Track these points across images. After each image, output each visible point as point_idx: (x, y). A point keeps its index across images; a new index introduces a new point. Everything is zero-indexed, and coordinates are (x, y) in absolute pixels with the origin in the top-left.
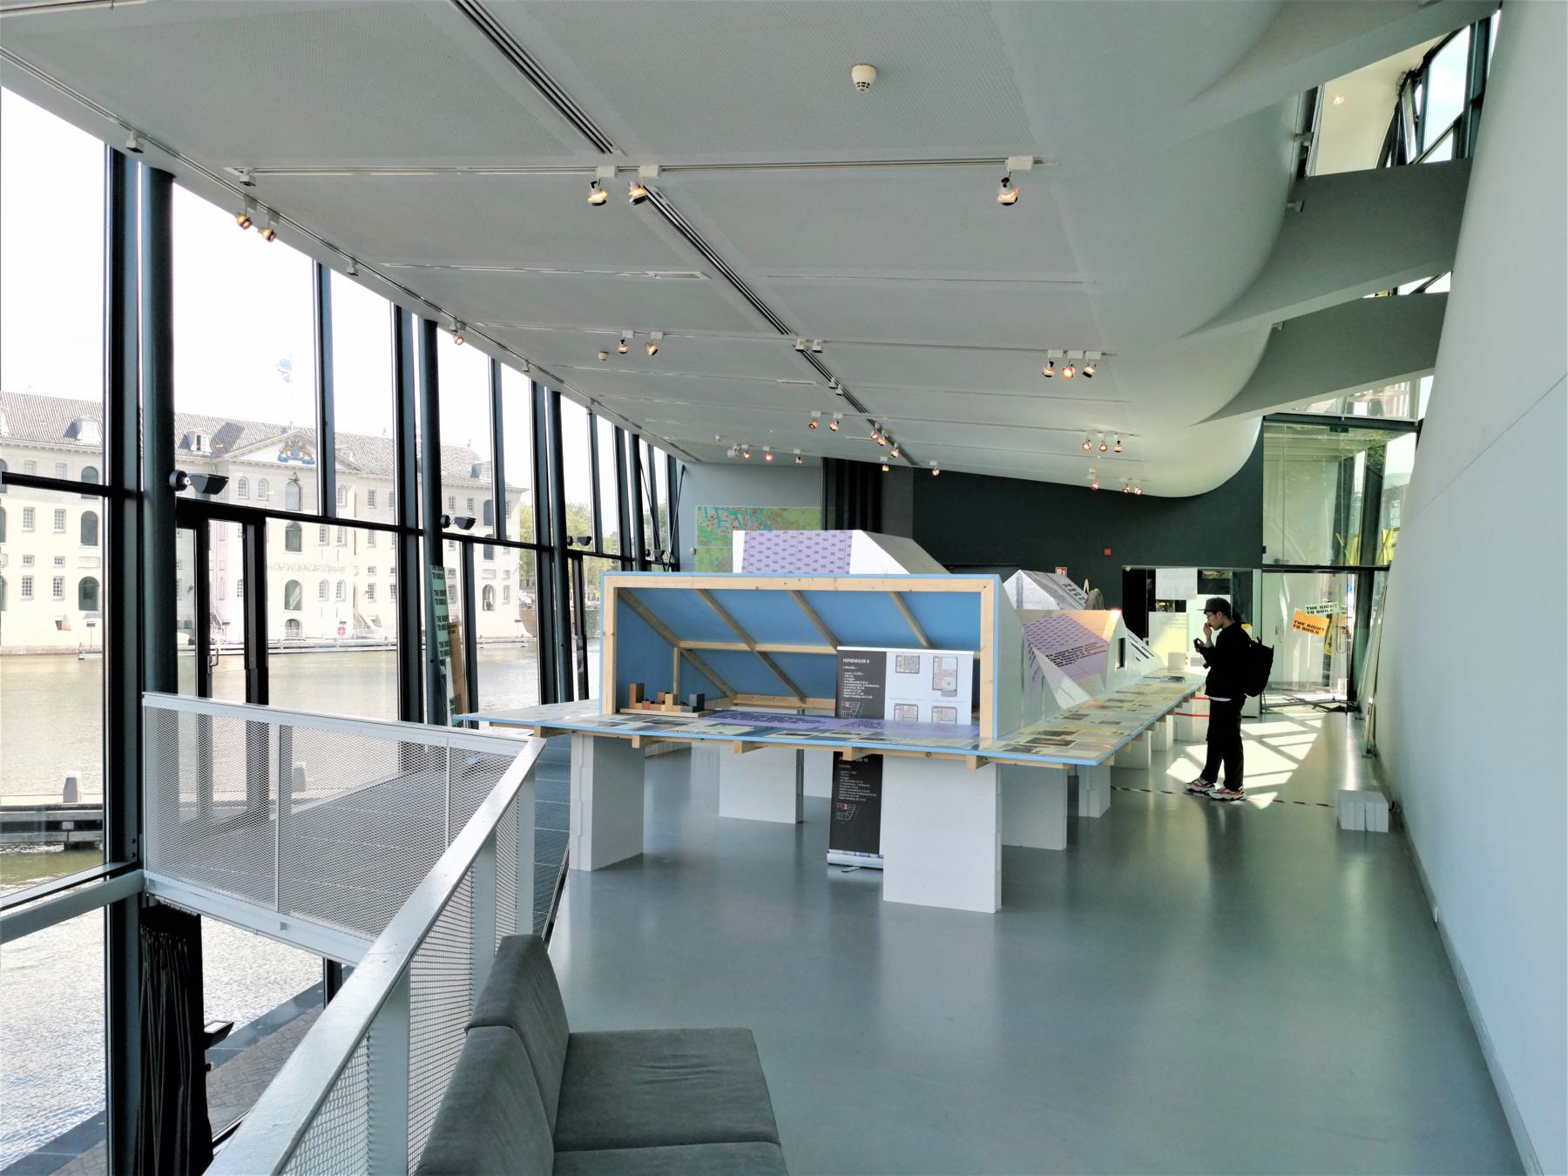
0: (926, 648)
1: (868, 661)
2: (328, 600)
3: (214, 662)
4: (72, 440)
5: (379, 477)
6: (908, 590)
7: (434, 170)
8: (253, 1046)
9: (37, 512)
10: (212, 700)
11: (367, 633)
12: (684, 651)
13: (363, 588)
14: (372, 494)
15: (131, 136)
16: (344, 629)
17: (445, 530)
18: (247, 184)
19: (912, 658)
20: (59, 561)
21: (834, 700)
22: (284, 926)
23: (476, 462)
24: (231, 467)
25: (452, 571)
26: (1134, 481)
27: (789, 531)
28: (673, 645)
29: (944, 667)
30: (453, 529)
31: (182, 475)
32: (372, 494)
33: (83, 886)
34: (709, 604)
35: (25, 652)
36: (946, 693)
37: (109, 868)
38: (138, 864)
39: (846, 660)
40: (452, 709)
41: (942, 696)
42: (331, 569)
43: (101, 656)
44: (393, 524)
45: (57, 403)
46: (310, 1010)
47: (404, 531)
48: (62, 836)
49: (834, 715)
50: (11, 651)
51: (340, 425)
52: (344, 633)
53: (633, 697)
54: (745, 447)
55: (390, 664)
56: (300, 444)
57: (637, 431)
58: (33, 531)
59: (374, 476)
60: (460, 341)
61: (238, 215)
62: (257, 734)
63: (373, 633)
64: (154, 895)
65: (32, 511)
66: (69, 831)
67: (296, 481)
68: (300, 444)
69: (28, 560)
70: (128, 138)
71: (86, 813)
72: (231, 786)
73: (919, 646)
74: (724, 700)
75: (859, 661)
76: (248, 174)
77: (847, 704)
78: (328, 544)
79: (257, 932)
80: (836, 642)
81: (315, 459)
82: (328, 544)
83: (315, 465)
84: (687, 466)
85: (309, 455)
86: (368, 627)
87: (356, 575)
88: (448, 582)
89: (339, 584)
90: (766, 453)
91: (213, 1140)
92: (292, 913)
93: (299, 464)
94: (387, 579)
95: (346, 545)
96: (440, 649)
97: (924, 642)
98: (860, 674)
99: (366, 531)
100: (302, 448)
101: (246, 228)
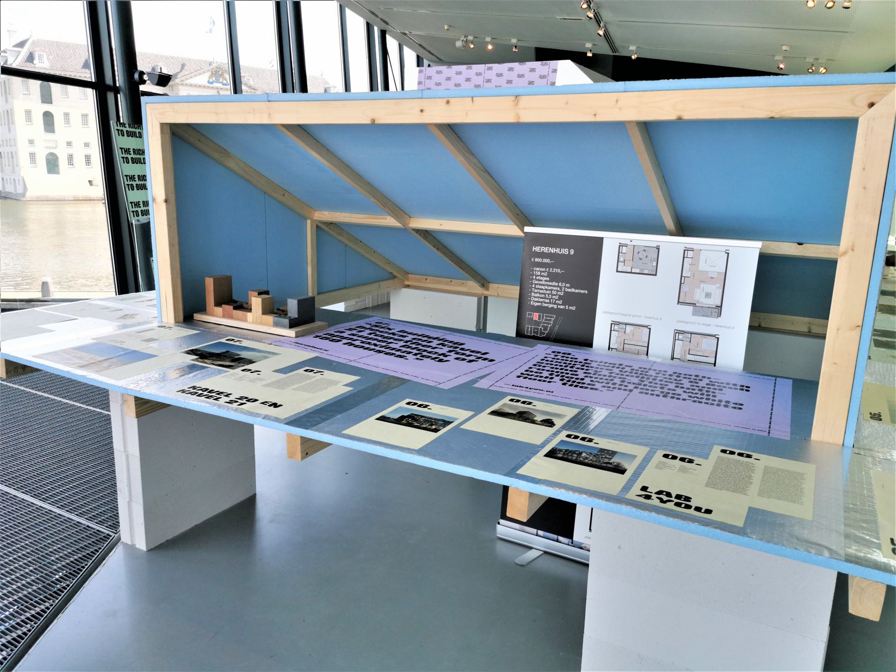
0: (671, 234)
1: (572, 252)
6: (672, 116)
12: (320, 225)
17: (142, 88)
19: (645, 249)
21: (518, 288)
23: (327, 86)
24: (181, 87)
26: (820, 61)
27: (474, 66)
28: (305, 219)
29: (702, 266)
34: (314, 155)
35: (73, 199)
36: (699, 310)
39: (537, 249)
41: (693, 314)
49: (513, 334)
50: (64, 198)
51: (244, 61)
53: (210, 298)
54: (470, 38)
56: (220, 73)
57: (384, 27)
65: (86, 116)
68: (220, 73)
73: (658, 229)
74: (391, 281)
75: (558, 250)
77: (535, 316)
80: (523, 219)
81: (229, 83)
83: (229, 87)
84: (431, 64)
85: (226, 80)
90: (487, 43)
93: (220, 85)
97: (670, 224)
98: (559, 271)
100: (221, 75)
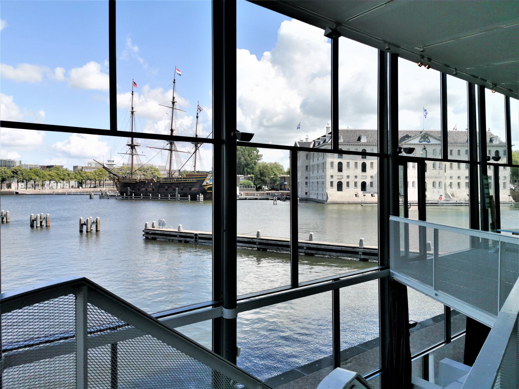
2: (436, 188)
3: (409, 207)
4: (359, 142)
5: (454, 145)
7: (485, 31)
8: (418, 331)
9: (358, 163)
10: (408, 218)
11: (450, 199)
13: (448, 184)
14: (459, 151)
15: (387, 45)
16: (441, 198)
17: (488, 162)
18: (422, 51)
20: (356, 177)
22: (436, 295)
23: (492, 137)
25: (490, 177)
30: (492, 161)
31: (401, 148)
32: (459, 151)
33: (366, 273)
37: (380, 267)
38: (388, 267)
40: (491, 227)
42: (436, 178)
43: (377, 204)
44: (468, 160)
45: (355, 131)
46: (437, 324)
47: (472, 164)
48: (359, 256)
51: (450, 128)
52: (441, 199)
55: (466, 210)
56: (426, 136)
58: (349, 169)
59: (452, 145)
60: (494, 91)
61: (418, 63)
62: (423, 231)
63: (451, 199)
64: (393, 278)
66: (361, 255)
67: (425, 149)
69: (348, 177)
70: (386, 46)
71: (371, 251)
72: (414, 248)
76: (423, 48)
78: (436, 169)
79: (427, 295)
82: (436, 169)
86: (450, 197)
87: (446, 179)
88: (489, 181)
89: (440, 183)
91: (412, 357)
92: (439, 291)
94: (465, 181)
95: (442, 169)
96: (486, 205)
99: (456, 164)
100: (427, 137)
101: (420, 66)
